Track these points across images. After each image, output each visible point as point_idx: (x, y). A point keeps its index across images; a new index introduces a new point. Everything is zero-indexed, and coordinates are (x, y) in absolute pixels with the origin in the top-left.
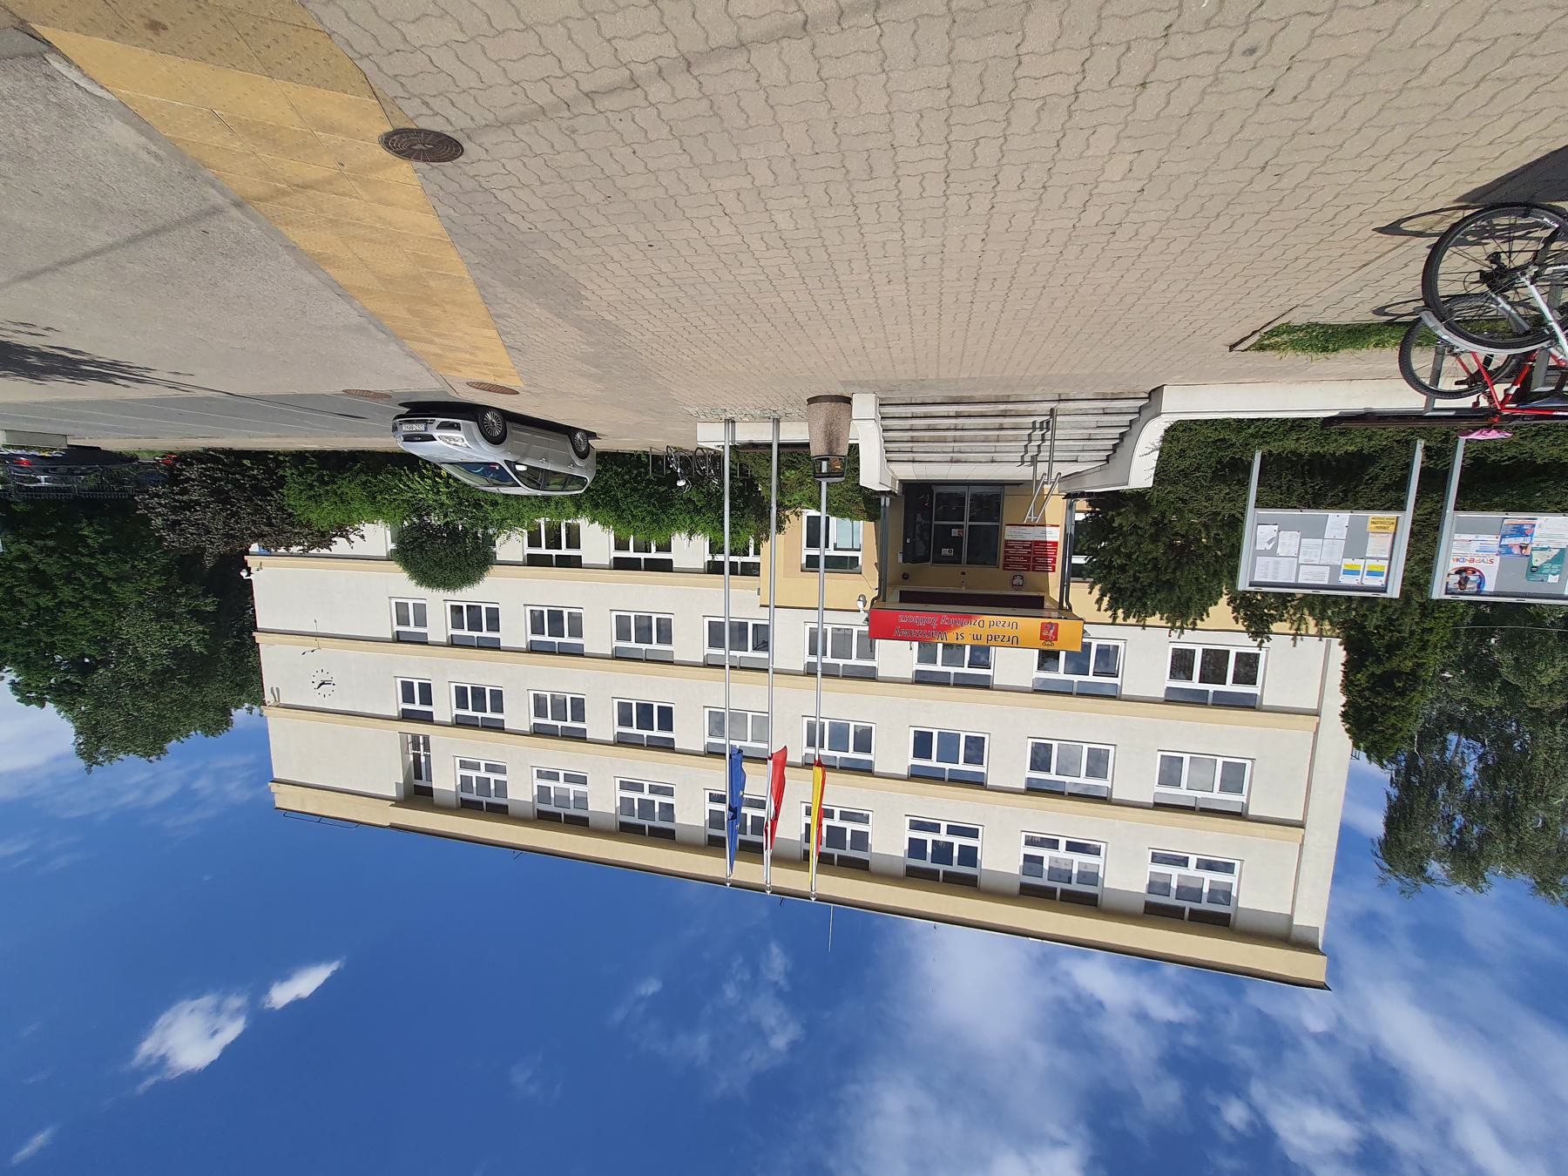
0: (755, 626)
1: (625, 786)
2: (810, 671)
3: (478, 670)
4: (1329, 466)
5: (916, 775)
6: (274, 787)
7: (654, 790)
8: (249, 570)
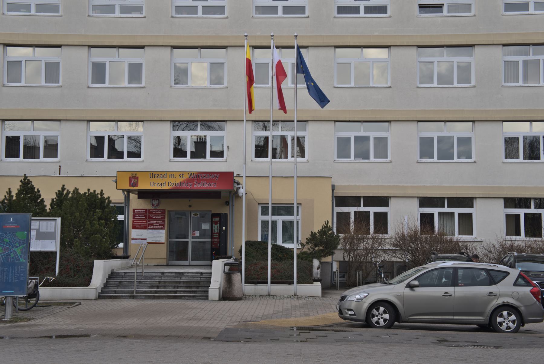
0: (103, 156)
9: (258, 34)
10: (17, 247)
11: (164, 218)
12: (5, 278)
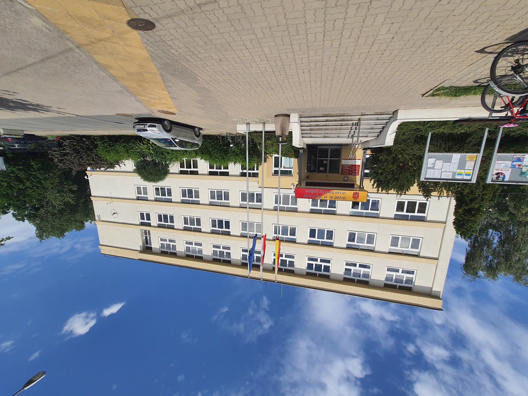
1: (310, 259)
2: (397, 218)
4: (454, 138)
5: (310, 243)
6: (100, 247)
7: (224, 248)
8: (87, 176)
11: (342, 170)
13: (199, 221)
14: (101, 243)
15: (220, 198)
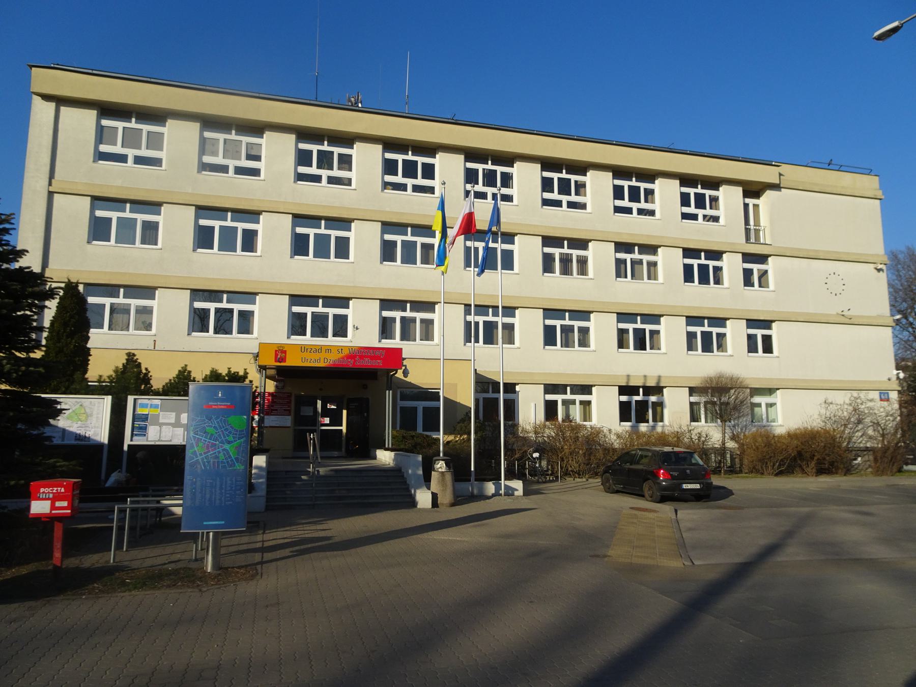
0: (555, 345)
2: (250, 296)
3: (702, 298)
6: (879, 194)
8: (898, 378)
9: (388, 209)
10: (229, 442)
11: (290, 402)
12: (208, 496)
13: (548, 264)
14: (878, 201)
15: (564, 327)
